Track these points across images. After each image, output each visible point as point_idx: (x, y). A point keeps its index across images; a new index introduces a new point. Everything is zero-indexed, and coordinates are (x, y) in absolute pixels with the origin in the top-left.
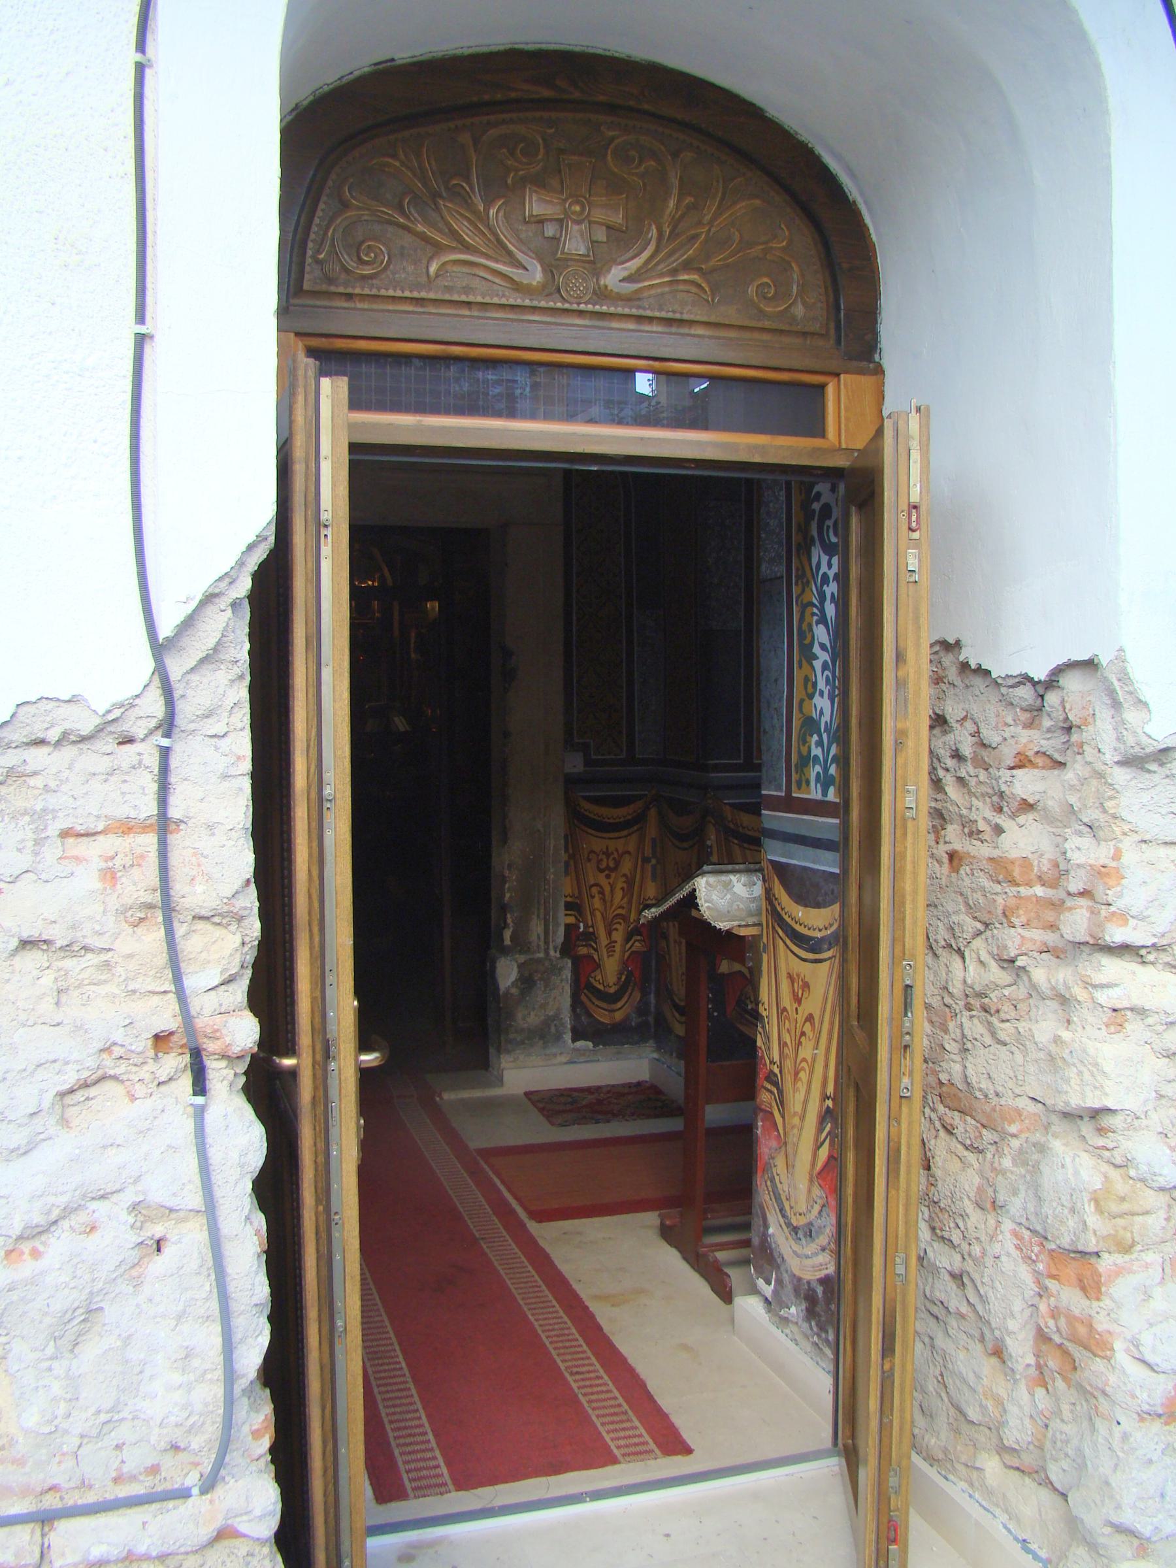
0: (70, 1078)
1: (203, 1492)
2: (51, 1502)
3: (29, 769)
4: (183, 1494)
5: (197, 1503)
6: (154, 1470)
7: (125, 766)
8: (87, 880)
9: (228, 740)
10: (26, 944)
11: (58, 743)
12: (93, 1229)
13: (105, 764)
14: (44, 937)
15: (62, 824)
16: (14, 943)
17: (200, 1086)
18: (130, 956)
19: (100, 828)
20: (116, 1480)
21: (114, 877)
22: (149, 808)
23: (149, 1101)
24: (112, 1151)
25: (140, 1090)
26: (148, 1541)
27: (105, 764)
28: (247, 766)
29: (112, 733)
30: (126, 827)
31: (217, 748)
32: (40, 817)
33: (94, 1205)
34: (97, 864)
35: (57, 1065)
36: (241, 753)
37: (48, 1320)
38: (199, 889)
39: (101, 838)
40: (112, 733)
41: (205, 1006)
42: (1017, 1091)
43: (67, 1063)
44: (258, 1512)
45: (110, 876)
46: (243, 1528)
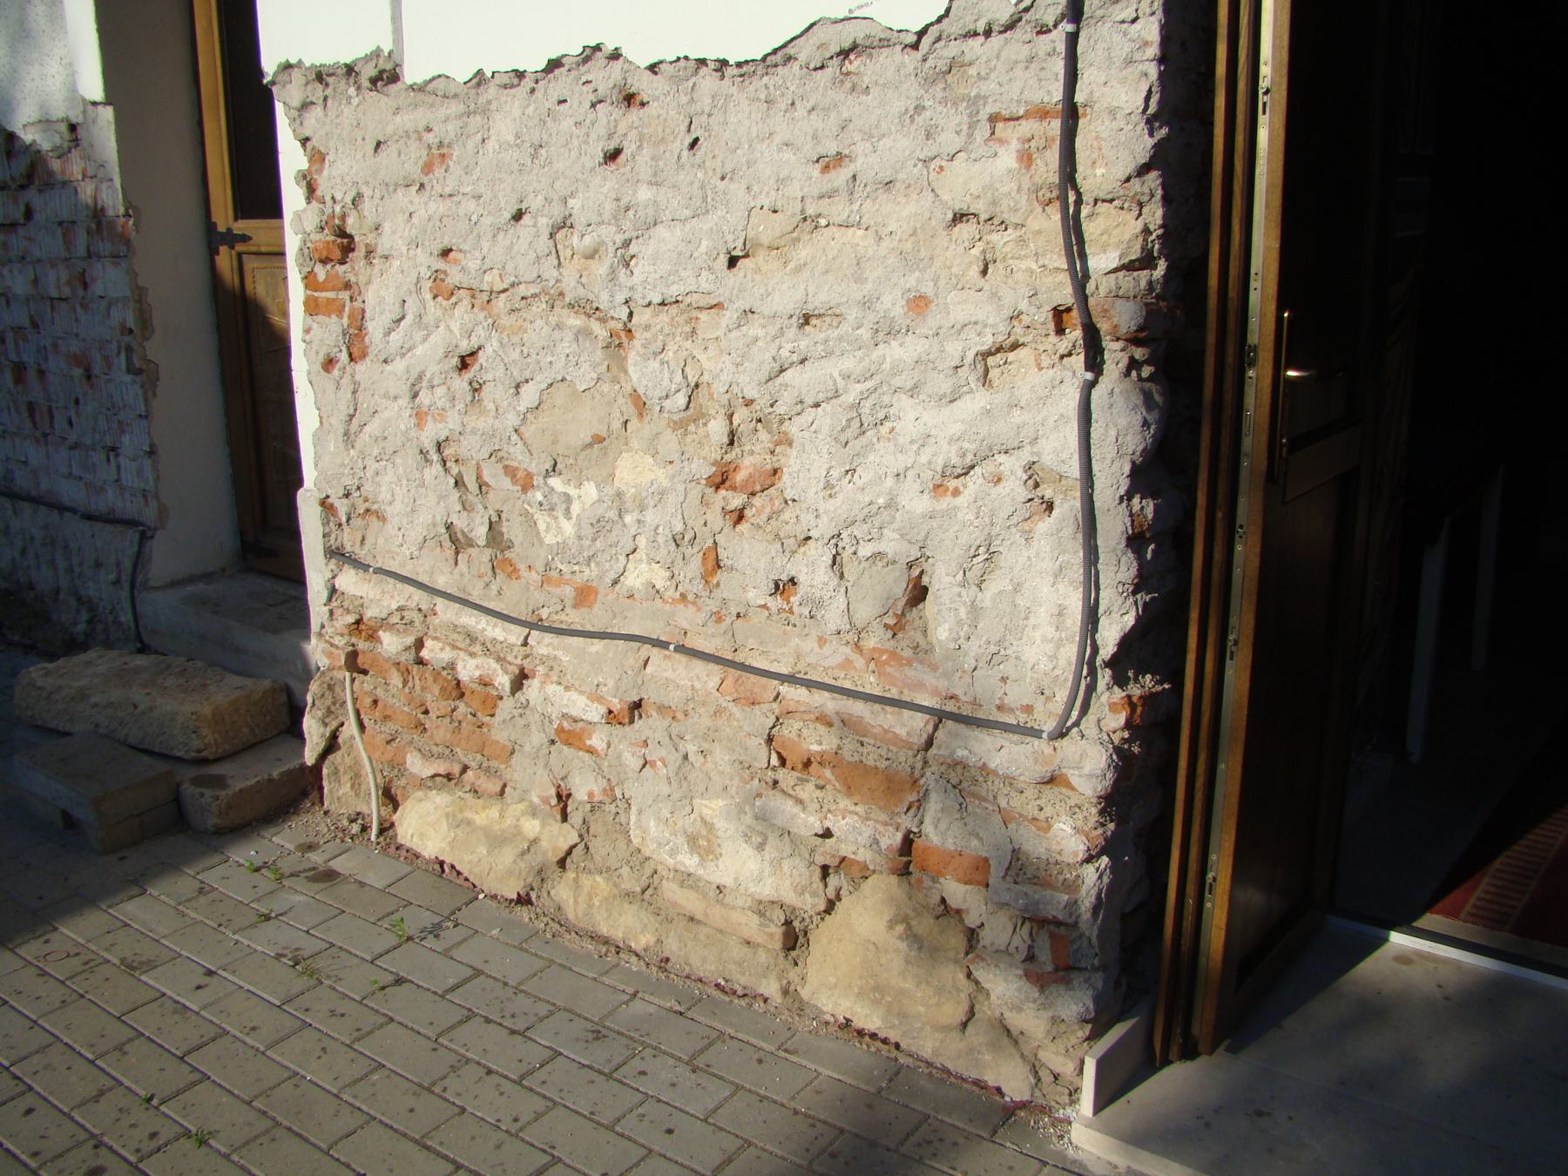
0: (987, 342)
1: (513, 693)
2: (950, 707)
3: (967, 59)
4: (1036, 734)
5: (1042, 746)
6: (1028, 709)
7: (1041, 54)
8: (1007, 159)
9: (1137, 26)
10: (959, 217)
11: (988, 33)
12: (999, 480)
13: (1025, 51)
14: (972, 210)
15: (990, 109)
16: (950, 216)
17: (1095, 362)
18: (1039, 232)
19: (1021, 113)
20: (999, 708)
21: (1030, 158)
22: (1057, 93)
23: (1051, 372)
24: (1016, 412)
25: (1046, 362)
26: (998, 761)
27: (1025, 51)
28: (1153, 51)
29: (1028, 22)
30: (1042, 114)
31: (1125, 34)
32: (975, 102)
33: (1001, 458)
34: (1015, 145)
35: (978, 327)
36: (1150, 39)
37: (957, 551)
38: (1099, 172)
39: (1023, 122)
40: (1028, 22)
41: (1100, 286)
42: (76, 472)
43: (985, 326)
44: (1086, 770)
45: (1026, 158)
46: (1075, 781)
